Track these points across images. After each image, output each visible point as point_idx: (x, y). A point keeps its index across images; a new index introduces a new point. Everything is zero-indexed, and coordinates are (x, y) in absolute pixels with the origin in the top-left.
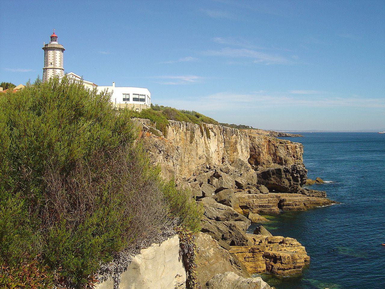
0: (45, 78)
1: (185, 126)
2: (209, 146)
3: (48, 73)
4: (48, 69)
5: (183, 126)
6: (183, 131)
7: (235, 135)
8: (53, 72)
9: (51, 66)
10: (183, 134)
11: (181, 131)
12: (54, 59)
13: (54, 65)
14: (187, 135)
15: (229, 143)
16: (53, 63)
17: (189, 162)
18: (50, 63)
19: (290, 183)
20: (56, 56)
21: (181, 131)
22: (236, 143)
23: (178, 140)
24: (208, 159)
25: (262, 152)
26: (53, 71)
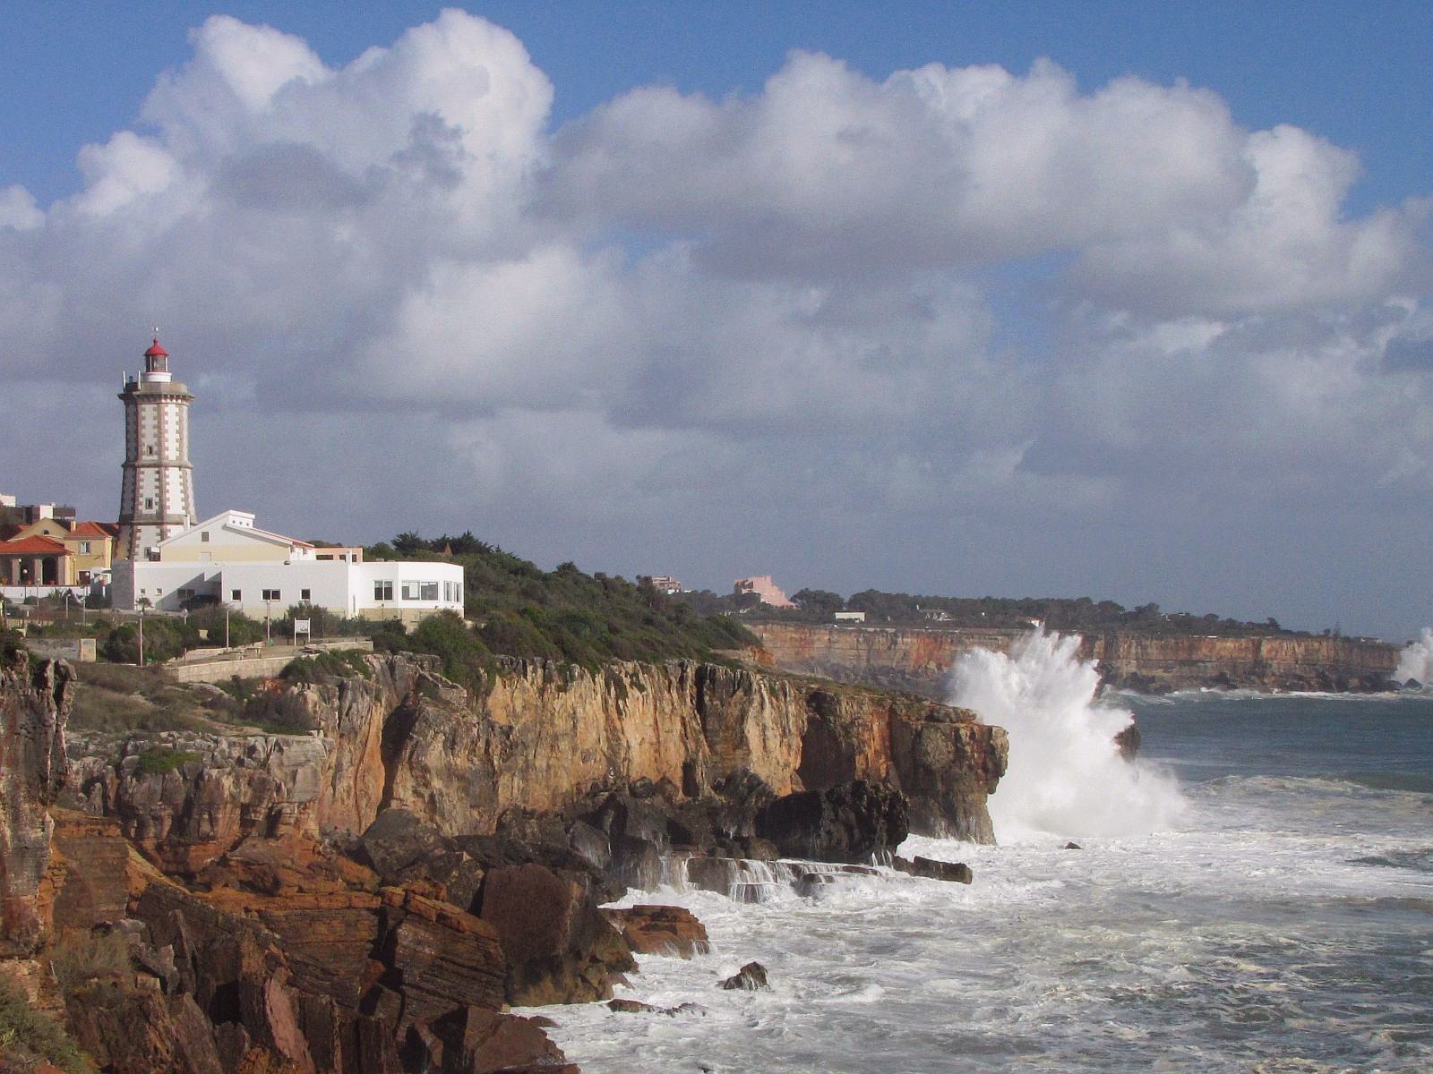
0: (133, 480)
1: (540, 671)
2: (619, 727)
3: (141, 483)
4: (139, 467)
5: (535, 671)
6: (532, 683)
7: (740, 693)
8: (157, 480)
9: (150, 458)
10: (533, 691)
11: (527, 684)
12: (161, 489)
13: (159, 453)
14: (545, 696)
15: (720, 717)
16: (155, 449)
17: (549, 767)
18: (145, 449)
19: (851, 836)
20: (167, 422)
21: (527, 684)
22: (742, 718)
23: (519, 710)
24: (611, 762)
25: (861, 752)
26: (157, 476)
